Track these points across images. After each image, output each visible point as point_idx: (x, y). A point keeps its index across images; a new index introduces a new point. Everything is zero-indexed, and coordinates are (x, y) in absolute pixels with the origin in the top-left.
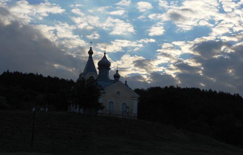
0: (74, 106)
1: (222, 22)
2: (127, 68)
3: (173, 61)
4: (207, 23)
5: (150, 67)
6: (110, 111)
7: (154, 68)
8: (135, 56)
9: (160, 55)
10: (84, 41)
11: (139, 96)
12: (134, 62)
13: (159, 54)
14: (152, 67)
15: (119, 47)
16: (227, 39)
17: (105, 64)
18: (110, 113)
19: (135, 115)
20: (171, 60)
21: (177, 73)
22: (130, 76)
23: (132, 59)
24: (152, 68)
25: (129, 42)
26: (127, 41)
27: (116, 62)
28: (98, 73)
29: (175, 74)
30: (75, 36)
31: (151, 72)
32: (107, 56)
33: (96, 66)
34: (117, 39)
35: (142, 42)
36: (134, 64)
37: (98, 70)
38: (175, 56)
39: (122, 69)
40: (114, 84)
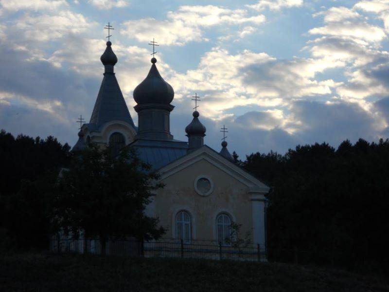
0: (70, 233)
2: (222, 91)
3: (361, 61)
5: (291, 82)
6: (182, 241)
7: (303, 87)
8: (243, 54)
9: (320, 44)
10: (85, 16)
11: (268, 188)
12: (242, 70)
13: (318, 40)
14: (298, 83)
15: (194, 27)
17: (155, 94)
18: (183, 248)
19: (259, 248)
20: (354, 59)
21: (376, 95)
22: (232, 115)
23: (234, 62)
24: (298, 88)
25: (222, 11)
26: (216, 8)
27: (186, 74)
28: (136, 124)
29: (367, 99)
31: (295, 98)
33: (131, 103)
34: (184, 5)
35: (263, 8)
36: (240, 78)
37: (133, 114)
38: (367, 47)
39: (206, 96)
40: (189, 157)
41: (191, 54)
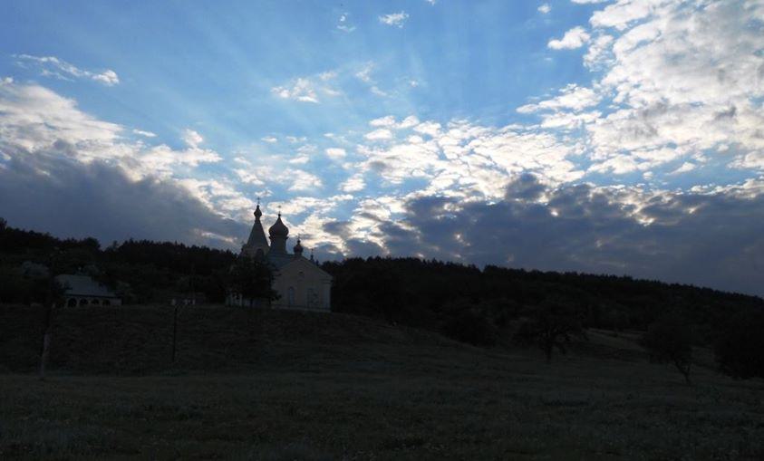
1: (445, 172)
4: (423, 174)
12: (324, 226)
16: (450, 194)
17: (279, 230)
23: (321, 222)
30: (237, 193)
32: (283, 219)
37: (269, 240)
41: (300, 218)
